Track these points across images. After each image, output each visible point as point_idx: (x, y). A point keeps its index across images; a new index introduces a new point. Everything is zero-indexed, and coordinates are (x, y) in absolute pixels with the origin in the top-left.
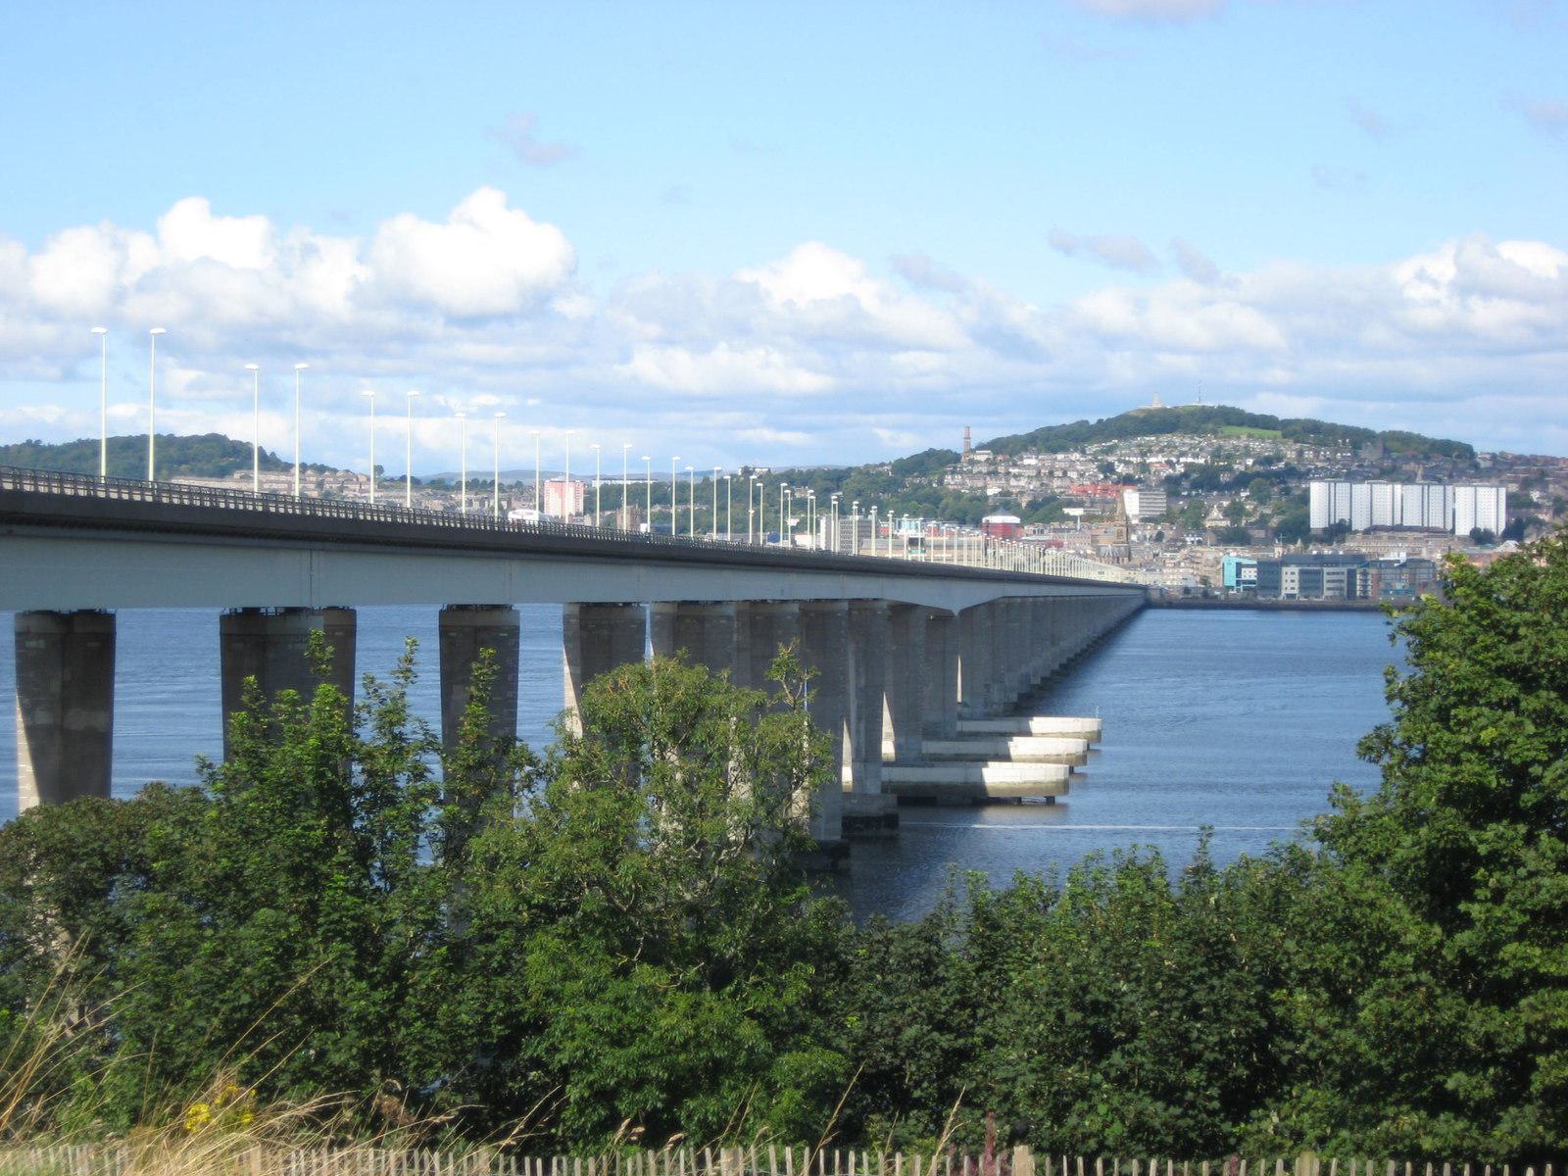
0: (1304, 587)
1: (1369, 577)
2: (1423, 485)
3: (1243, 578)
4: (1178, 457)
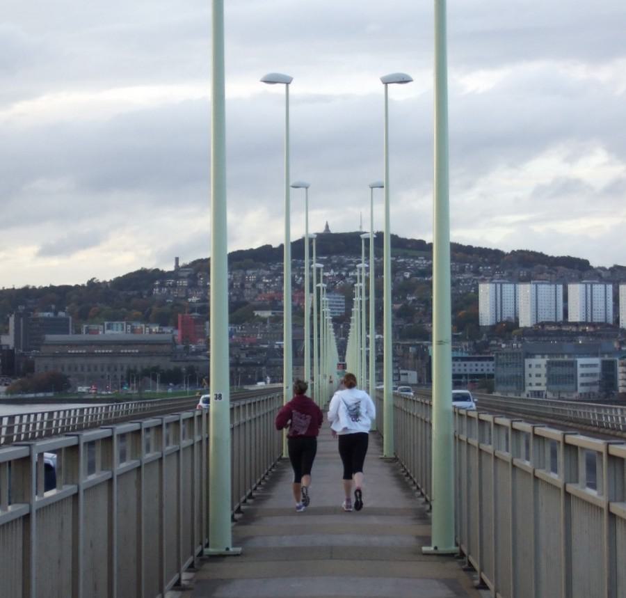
0: (552, 379)
2: (496, 283)
4: (348, 272)
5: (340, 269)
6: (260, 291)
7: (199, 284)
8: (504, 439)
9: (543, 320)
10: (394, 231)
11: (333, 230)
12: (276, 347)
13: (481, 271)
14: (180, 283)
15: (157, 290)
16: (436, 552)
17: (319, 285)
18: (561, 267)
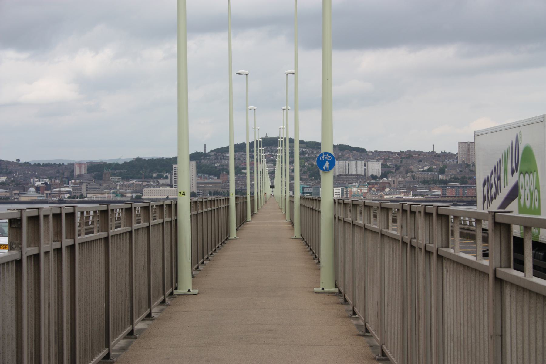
1: (348, 191)
3: (305, 192)
4: (275, 153)
8: (383, 219)
9: (341, 173)
11: (269, 136)
12: (252, 184)
14: (211, 157)
15: (203, 160)
16: (323, 291)
17: (260, 148)
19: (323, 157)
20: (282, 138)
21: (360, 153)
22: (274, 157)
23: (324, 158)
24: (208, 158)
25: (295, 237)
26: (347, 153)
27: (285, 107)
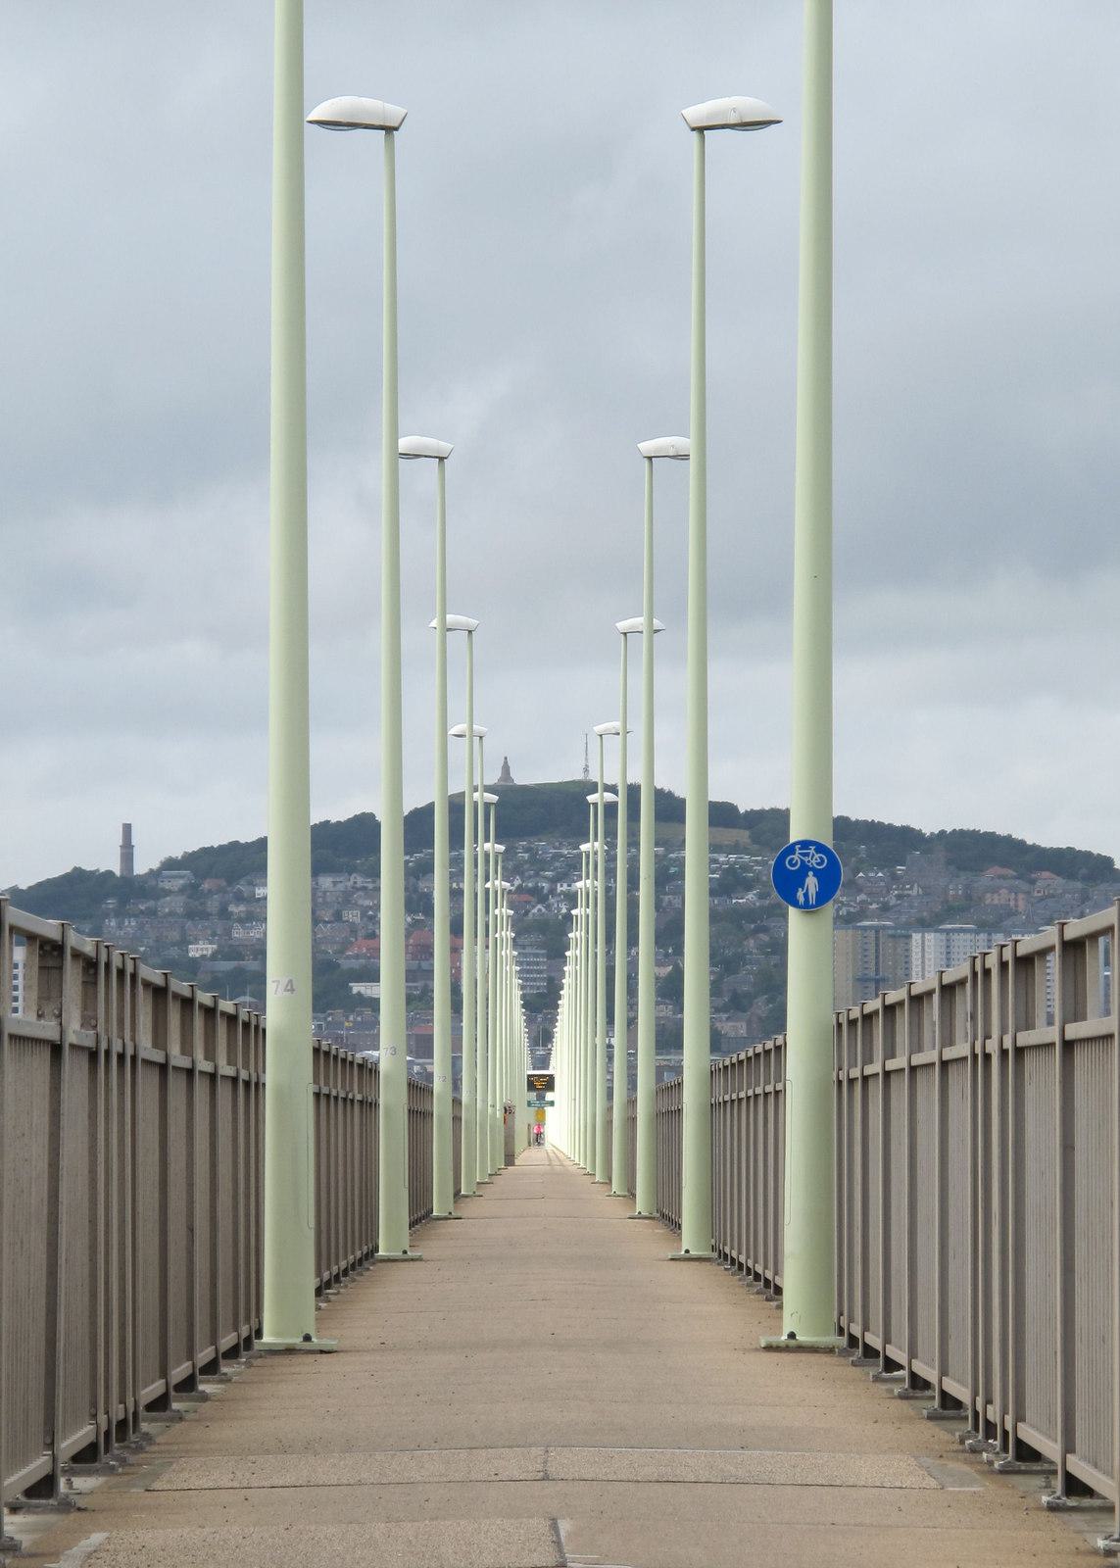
4: (554, 881)
5: (537, 874)
6: (353, 930)
7: (209, 910)
10: (662, 782)
13: (860, 882)
15: (113, 923)
18: (1046, 874)
19: (796, 857)
20: (613, 789)
21: (1079, 885)
22: (548, 907)
23: (802, 860)
24: (142, 907)
25: (687, 1251)
26: (998, 882)
27: (639, 622)
